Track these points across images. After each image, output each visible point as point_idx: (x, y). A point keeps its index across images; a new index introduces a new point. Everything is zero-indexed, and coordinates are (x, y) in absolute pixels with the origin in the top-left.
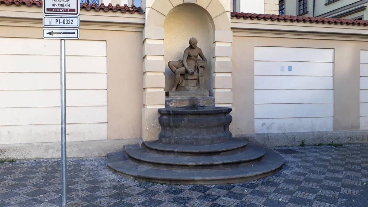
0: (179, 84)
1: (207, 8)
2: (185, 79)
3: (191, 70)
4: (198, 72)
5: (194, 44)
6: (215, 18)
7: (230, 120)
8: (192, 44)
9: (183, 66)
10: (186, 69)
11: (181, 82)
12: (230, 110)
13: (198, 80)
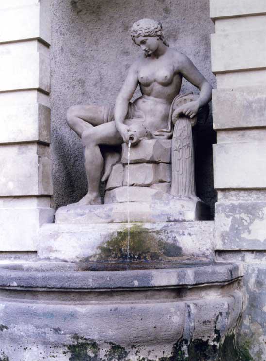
0: (104, 179)
5: (141, 39)
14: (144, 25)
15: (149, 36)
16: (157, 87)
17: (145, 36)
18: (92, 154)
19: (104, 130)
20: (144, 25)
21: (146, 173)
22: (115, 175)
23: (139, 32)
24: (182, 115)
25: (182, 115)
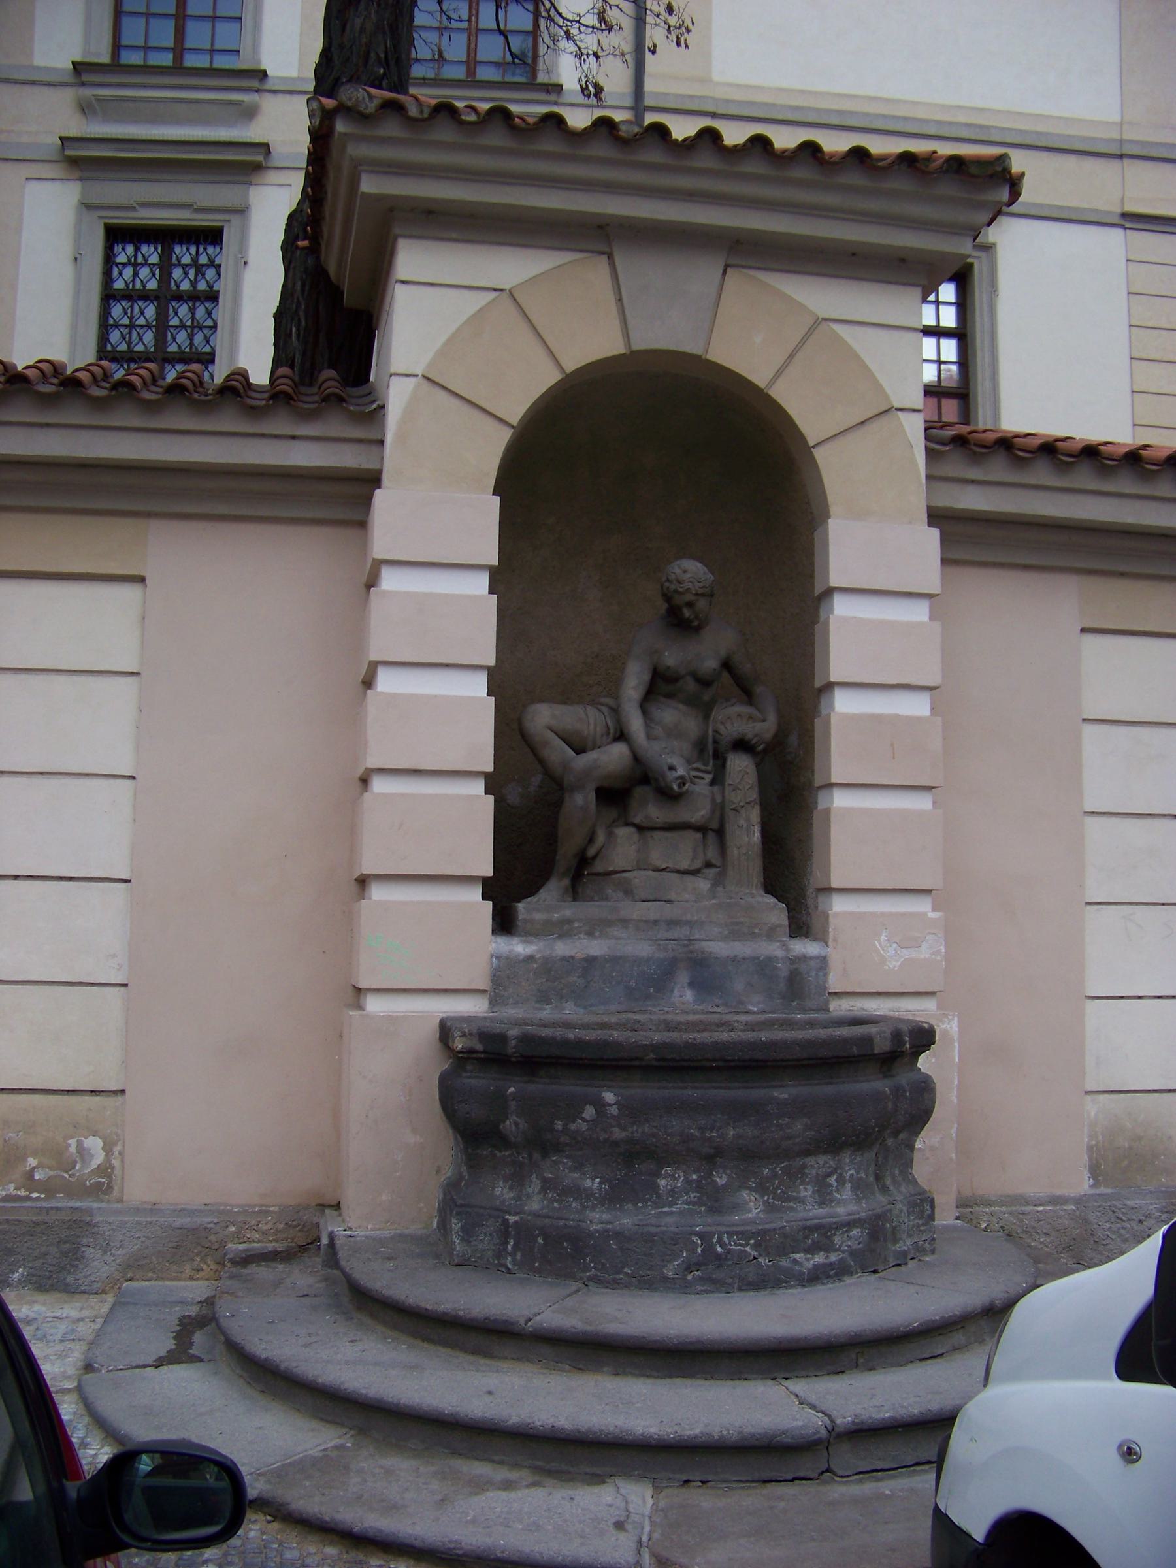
0: (591, 852)
1: (632, 341)
2: (627, 824)
3: (673, 760)
4: (718, 779)
5: (689, 597)
6: (403, 282)
7: (918, 1106)
8: (678, 600)
9: (621, 736)
10: (636, 758)
11: (601, 838)
12: (924, 1038)
13: (720, 833)
14: (690, 572)
15: (703, 595)
16: (690, 685)
17: (697, 594)
18: (582, 800)
19: (612, 758)
20: (690, 572)
21: (684, 850)
22: (622, 848)
23: (690, 586)
24: (742, 745)
25: (742, 745)
